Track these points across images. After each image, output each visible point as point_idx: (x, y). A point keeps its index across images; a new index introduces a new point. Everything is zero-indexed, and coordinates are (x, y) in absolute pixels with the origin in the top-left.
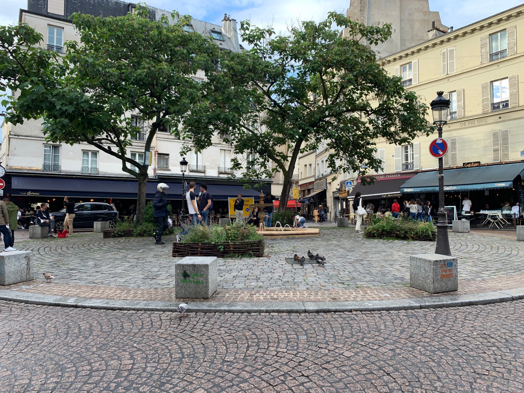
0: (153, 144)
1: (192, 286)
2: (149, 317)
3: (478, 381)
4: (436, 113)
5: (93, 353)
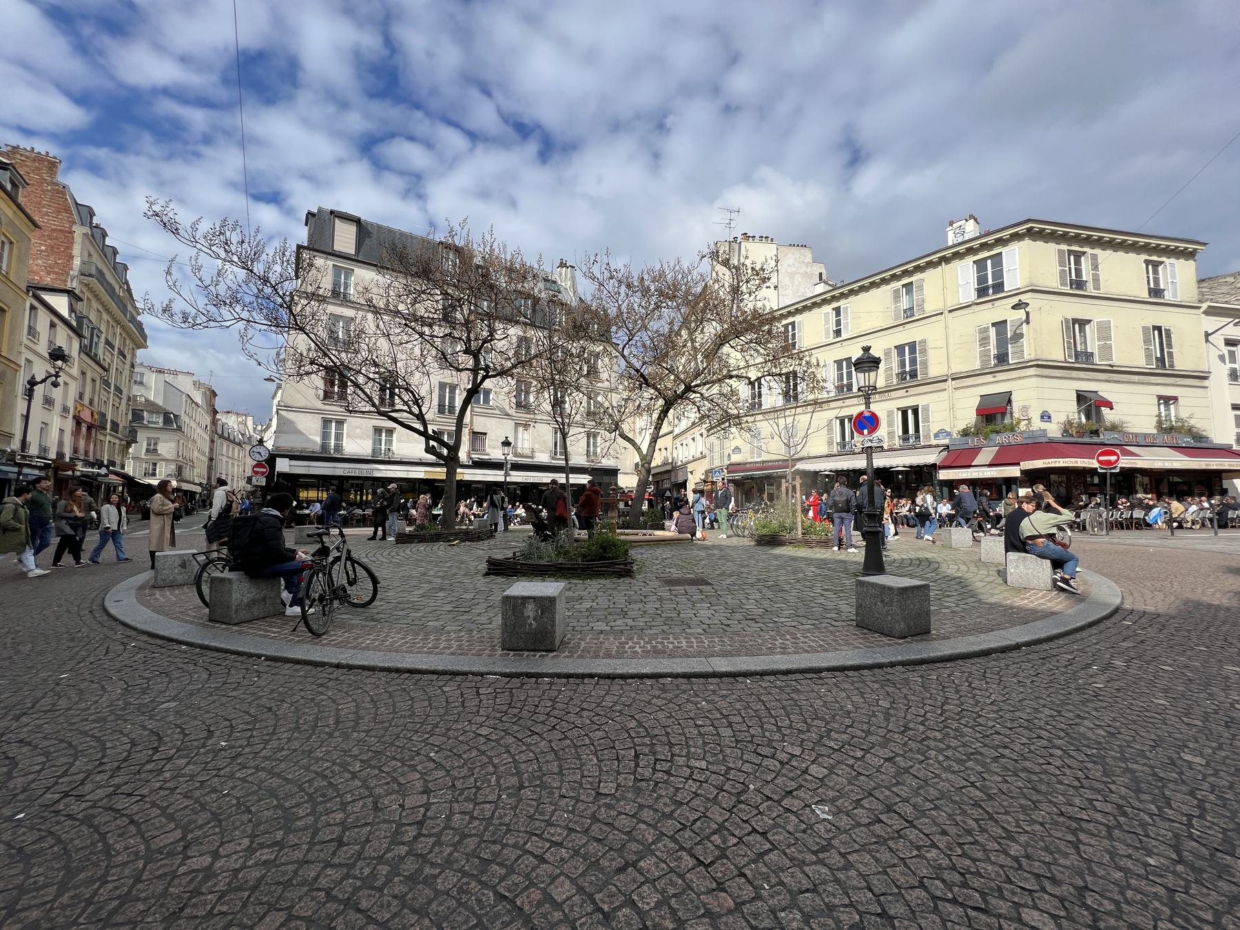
0: (467, 419)
1: (530, 633)
2: (459, 687)
3: (1044, 806)
4: (861, 375)
5: (354, 775)
